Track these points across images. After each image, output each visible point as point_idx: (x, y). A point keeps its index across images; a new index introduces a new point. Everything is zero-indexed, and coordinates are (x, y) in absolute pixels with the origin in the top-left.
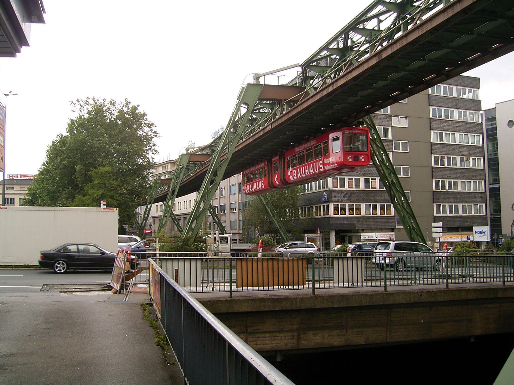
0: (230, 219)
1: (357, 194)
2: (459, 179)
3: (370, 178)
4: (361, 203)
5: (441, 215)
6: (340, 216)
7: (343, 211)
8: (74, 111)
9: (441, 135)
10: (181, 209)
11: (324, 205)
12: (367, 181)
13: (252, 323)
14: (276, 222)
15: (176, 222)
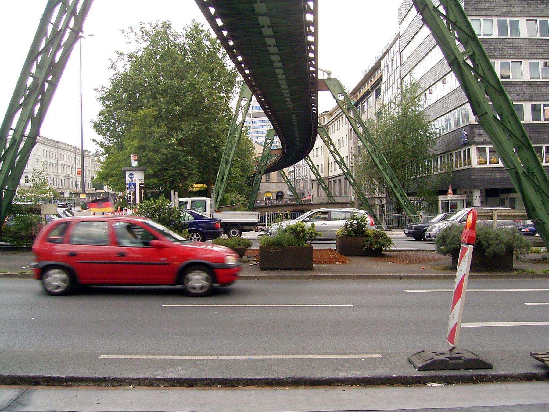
3: (542, 103)
8: (129, 43)
12: (535, 109)
14: (388, 178)
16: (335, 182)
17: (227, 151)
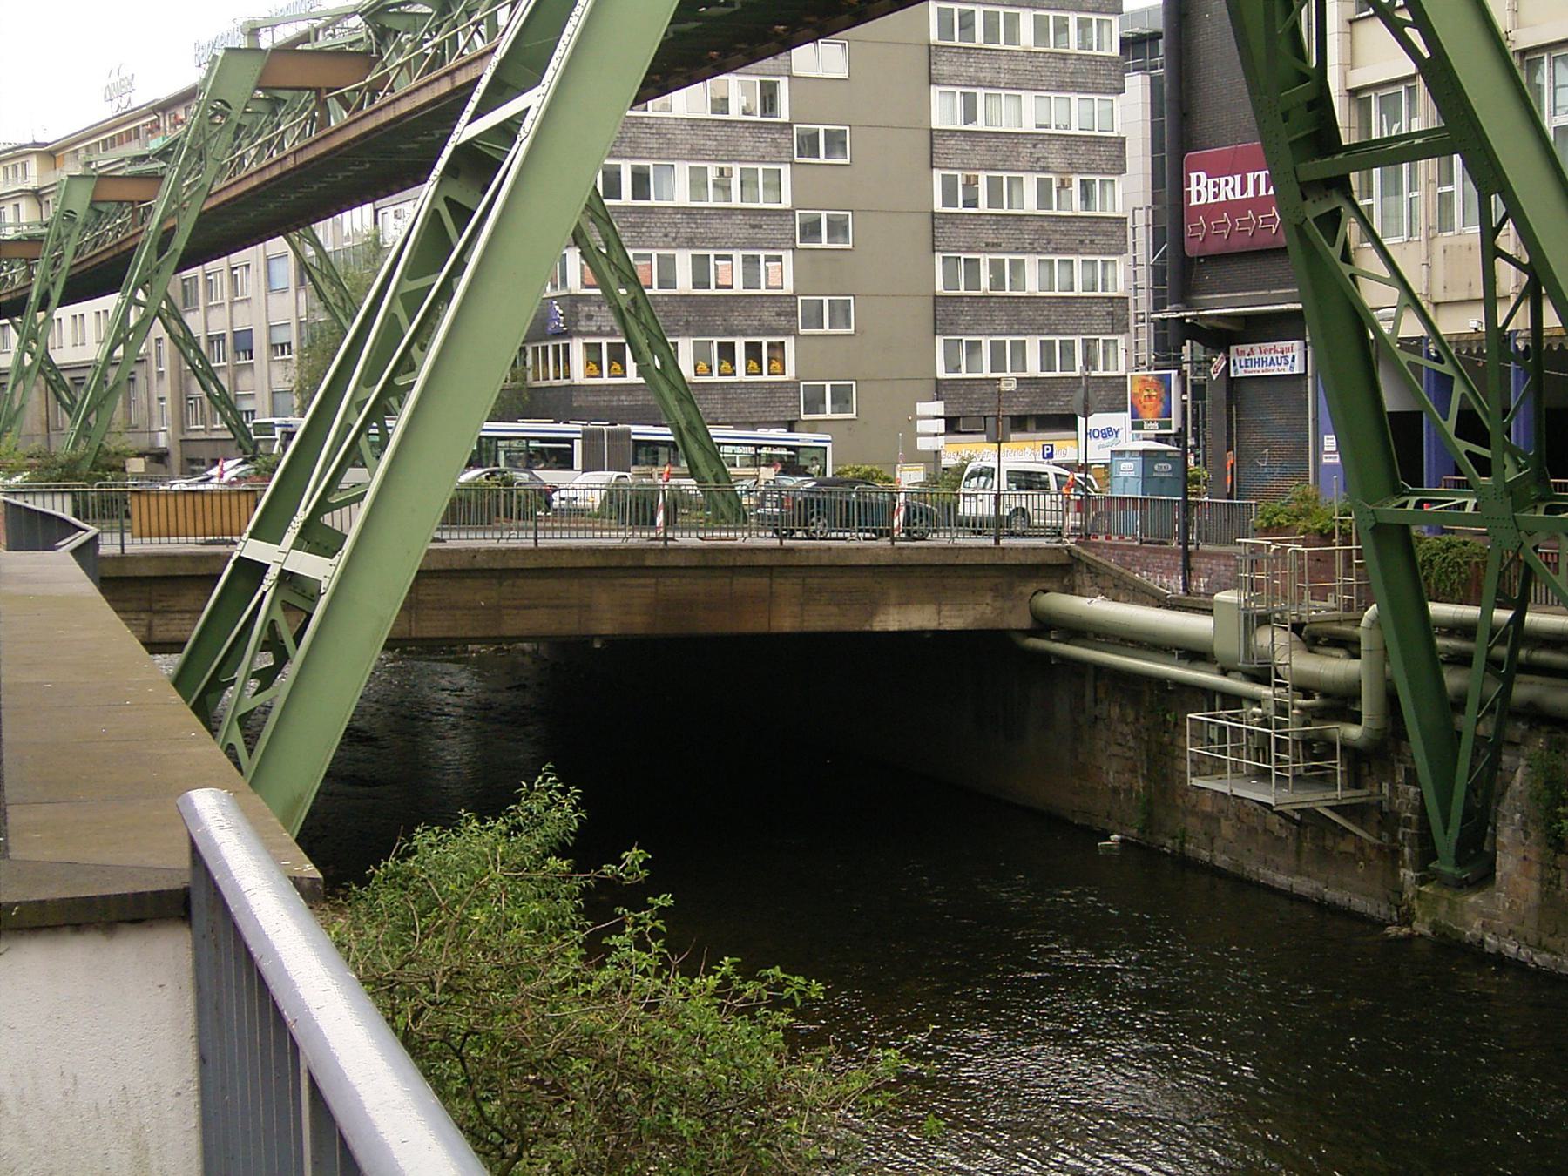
0: (270, 383)
1: (665, 308)
2: (1029, 252)
3: (712, 253)
4: (678, 336)
5: (963, 374)
9: (970, 101)
10: (83, 344)
11: (555, 343)
13: (161, 595)
15: (64, 394)
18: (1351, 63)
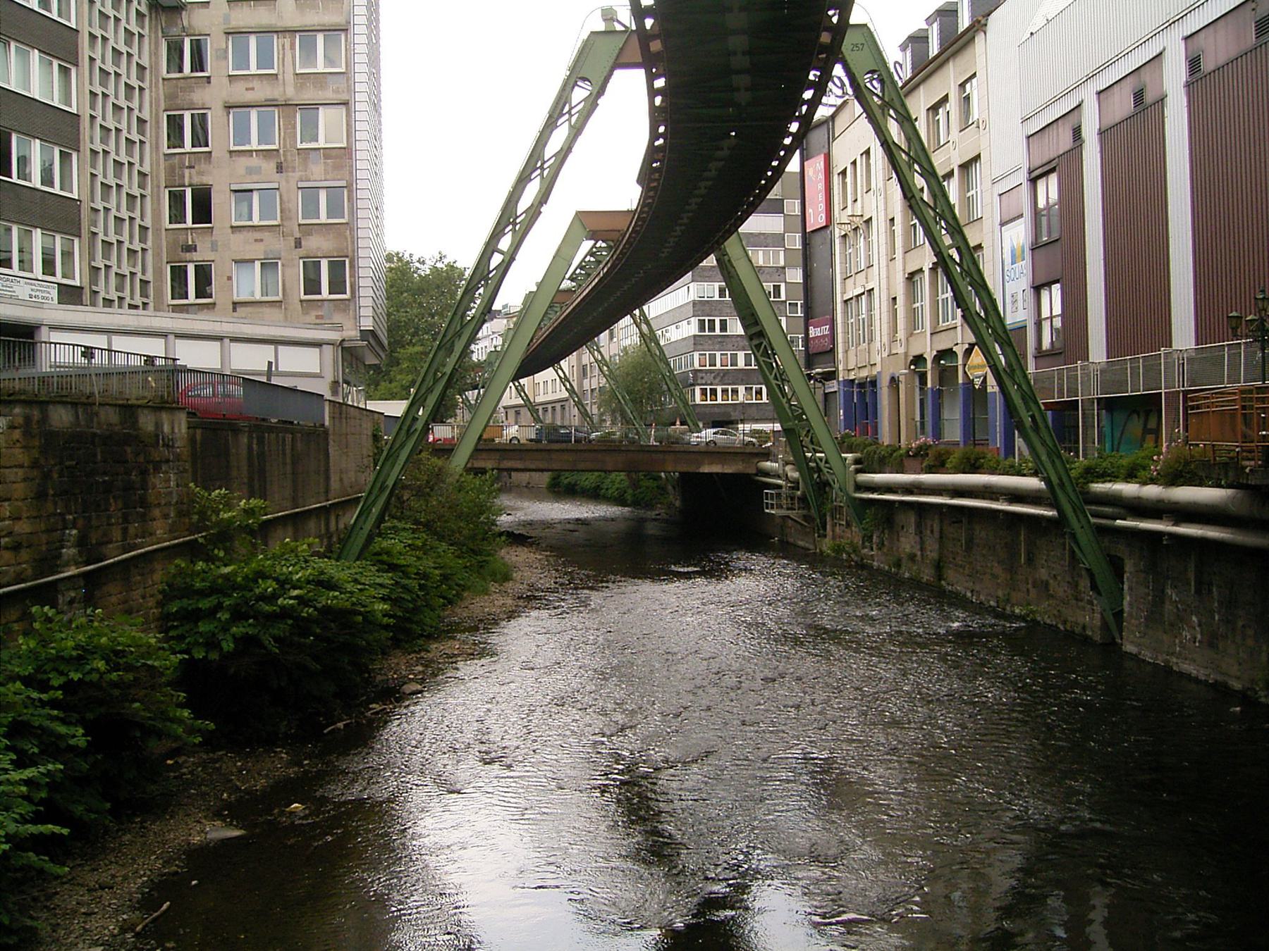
6: (709, 402)
7: (713, 397)
14: (629, 412)
16: (545, 410)
17: (445, 340)
18: (843, 293)
